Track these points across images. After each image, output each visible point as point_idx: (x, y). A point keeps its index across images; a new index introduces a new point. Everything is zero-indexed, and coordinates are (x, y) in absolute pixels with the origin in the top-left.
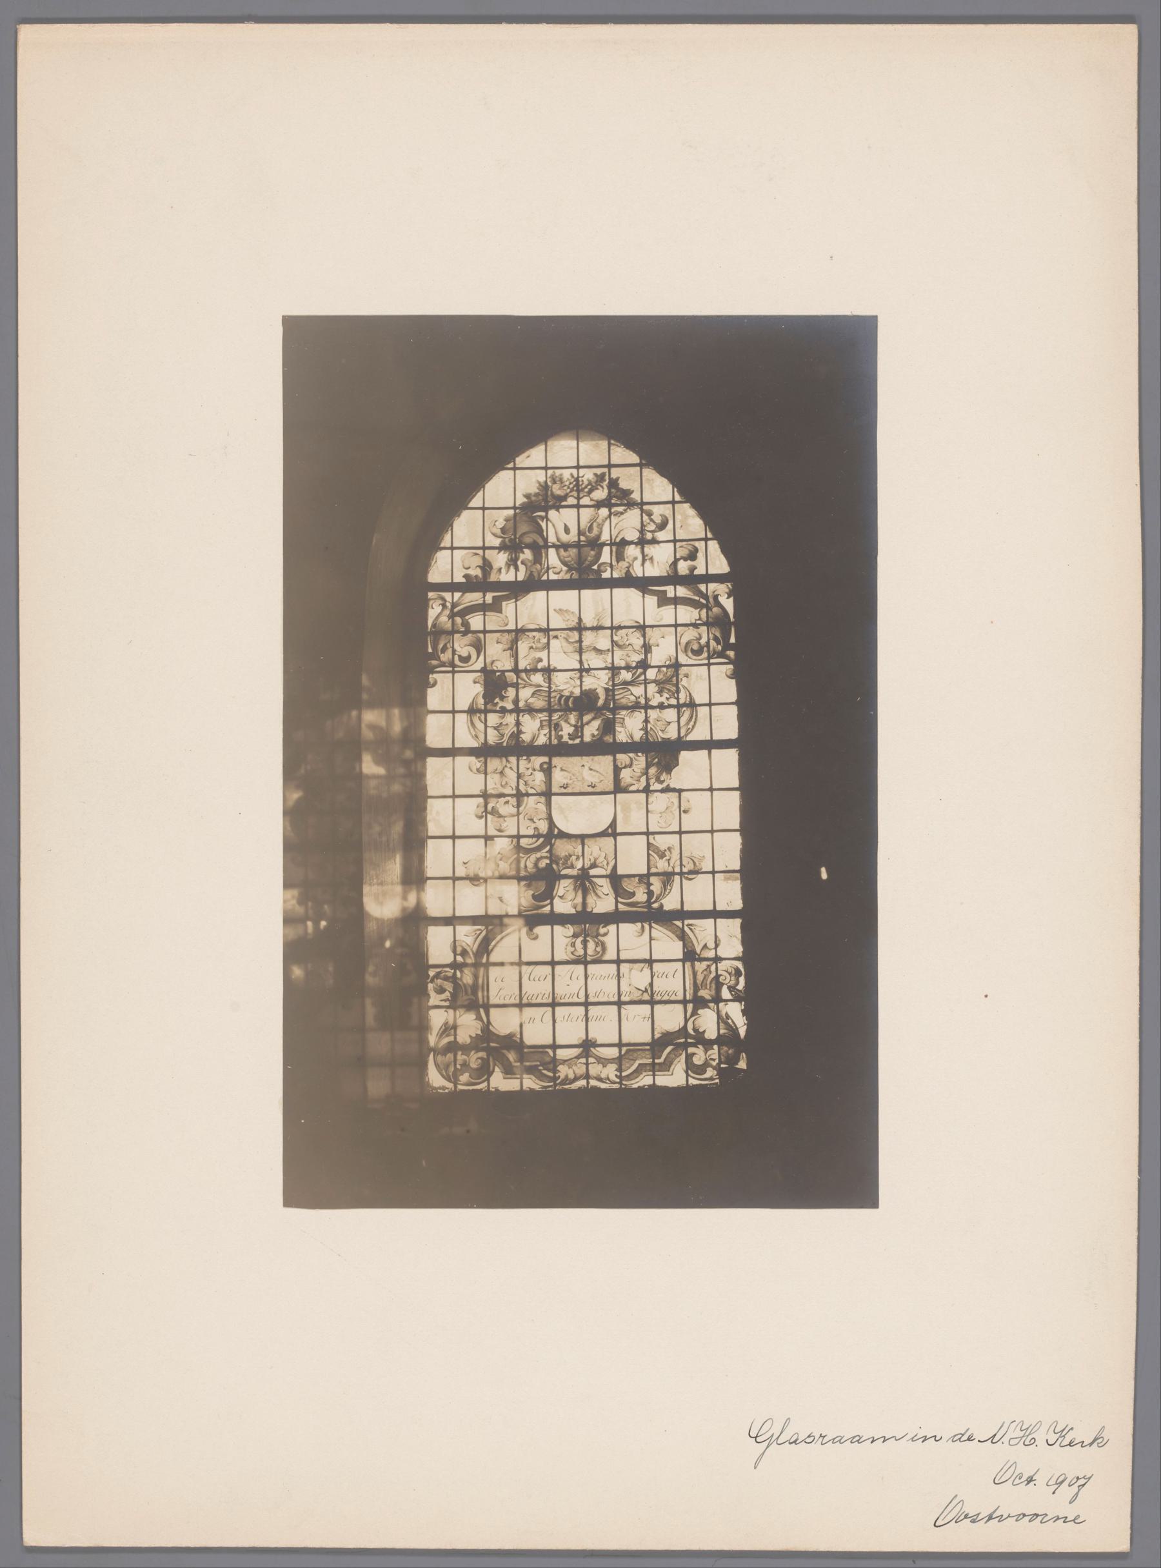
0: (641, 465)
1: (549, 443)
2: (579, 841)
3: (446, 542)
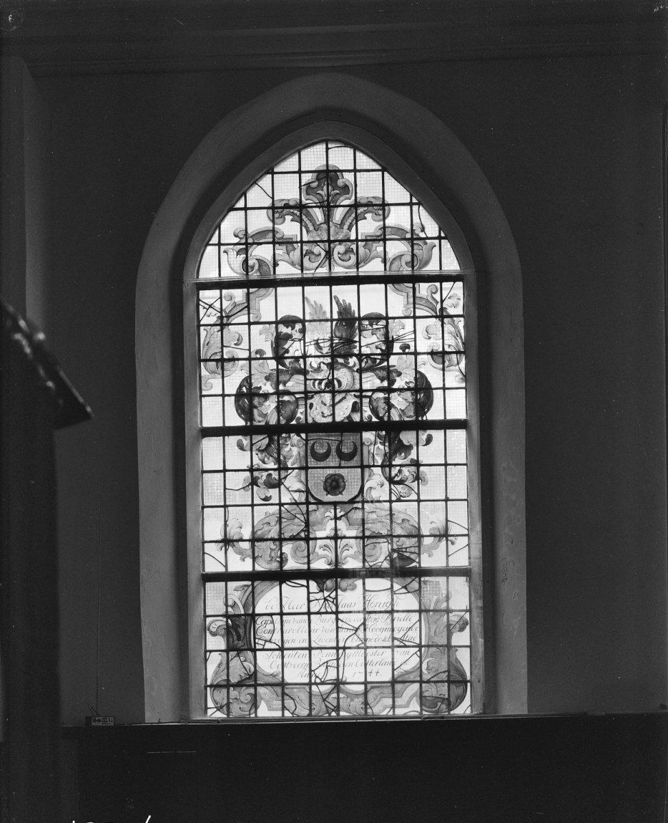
1: (303, 153)
2: (367, 593)
3: (215, 240)
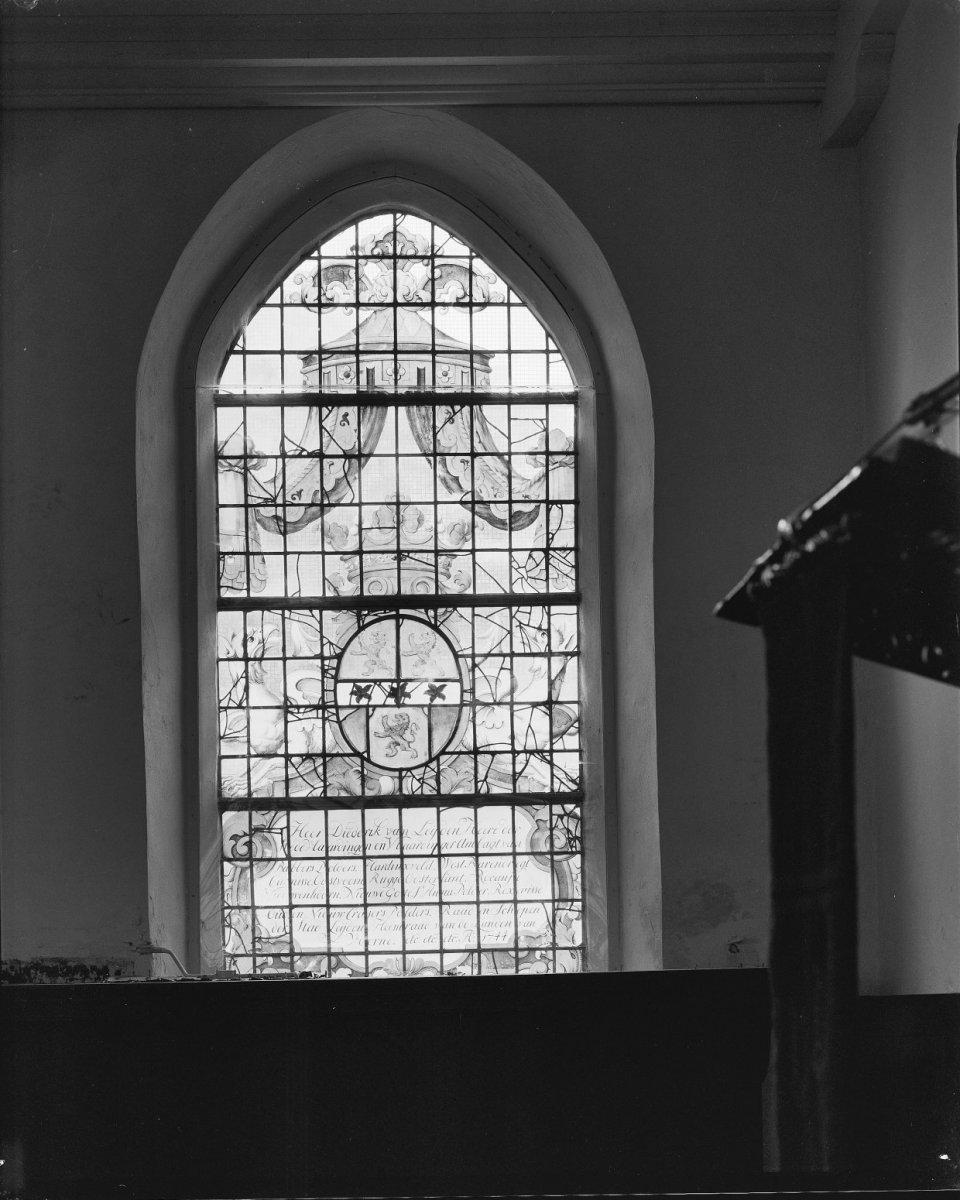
0: (547, 352)
